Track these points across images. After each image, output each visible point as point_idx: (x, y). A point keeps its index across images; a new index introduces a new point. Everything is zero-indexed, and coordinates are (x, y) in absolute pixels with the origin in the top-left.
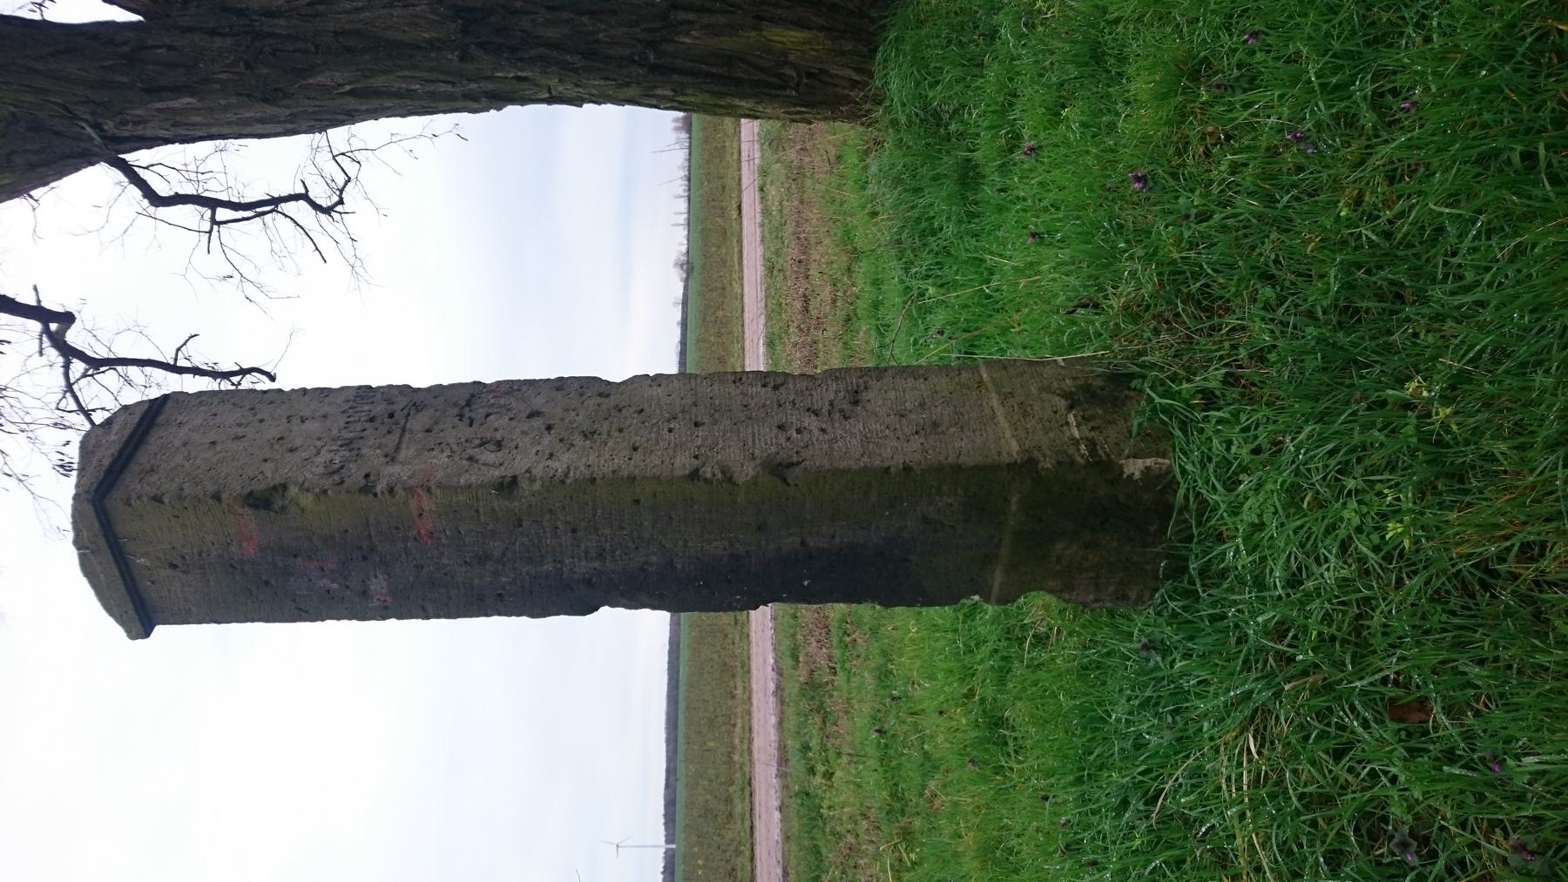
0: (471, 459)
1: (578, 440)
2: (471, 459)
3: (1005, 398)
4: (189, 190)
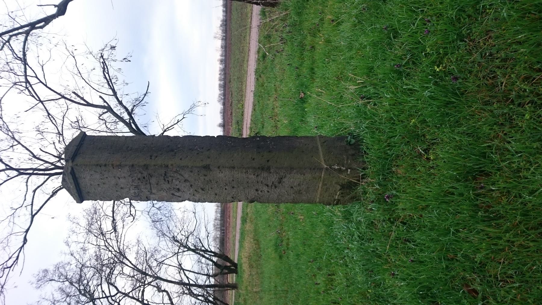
0: (173, 194)
1: (200, 191)
2: (173, 194)
3: (324, 185)
4: (36, 187)
